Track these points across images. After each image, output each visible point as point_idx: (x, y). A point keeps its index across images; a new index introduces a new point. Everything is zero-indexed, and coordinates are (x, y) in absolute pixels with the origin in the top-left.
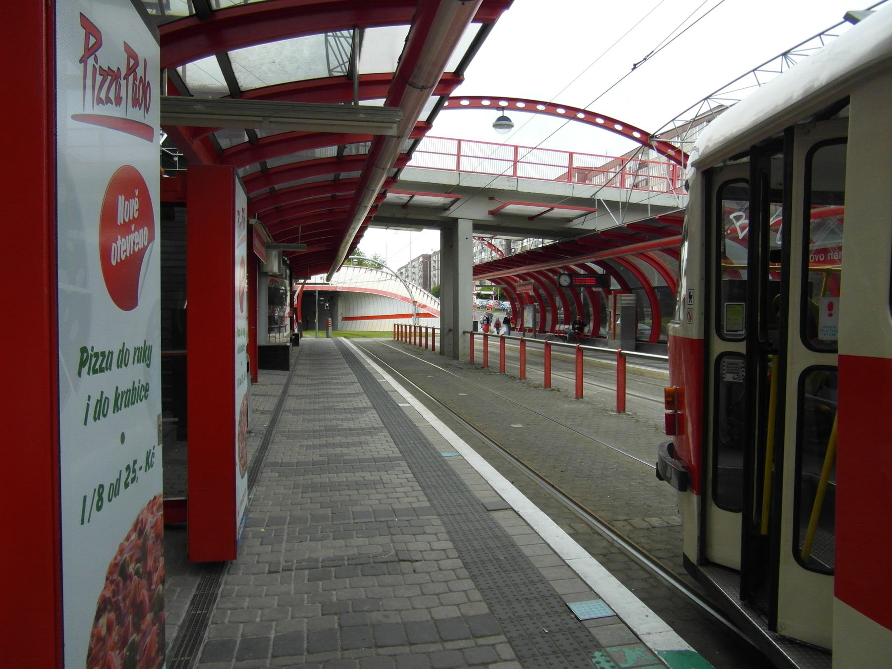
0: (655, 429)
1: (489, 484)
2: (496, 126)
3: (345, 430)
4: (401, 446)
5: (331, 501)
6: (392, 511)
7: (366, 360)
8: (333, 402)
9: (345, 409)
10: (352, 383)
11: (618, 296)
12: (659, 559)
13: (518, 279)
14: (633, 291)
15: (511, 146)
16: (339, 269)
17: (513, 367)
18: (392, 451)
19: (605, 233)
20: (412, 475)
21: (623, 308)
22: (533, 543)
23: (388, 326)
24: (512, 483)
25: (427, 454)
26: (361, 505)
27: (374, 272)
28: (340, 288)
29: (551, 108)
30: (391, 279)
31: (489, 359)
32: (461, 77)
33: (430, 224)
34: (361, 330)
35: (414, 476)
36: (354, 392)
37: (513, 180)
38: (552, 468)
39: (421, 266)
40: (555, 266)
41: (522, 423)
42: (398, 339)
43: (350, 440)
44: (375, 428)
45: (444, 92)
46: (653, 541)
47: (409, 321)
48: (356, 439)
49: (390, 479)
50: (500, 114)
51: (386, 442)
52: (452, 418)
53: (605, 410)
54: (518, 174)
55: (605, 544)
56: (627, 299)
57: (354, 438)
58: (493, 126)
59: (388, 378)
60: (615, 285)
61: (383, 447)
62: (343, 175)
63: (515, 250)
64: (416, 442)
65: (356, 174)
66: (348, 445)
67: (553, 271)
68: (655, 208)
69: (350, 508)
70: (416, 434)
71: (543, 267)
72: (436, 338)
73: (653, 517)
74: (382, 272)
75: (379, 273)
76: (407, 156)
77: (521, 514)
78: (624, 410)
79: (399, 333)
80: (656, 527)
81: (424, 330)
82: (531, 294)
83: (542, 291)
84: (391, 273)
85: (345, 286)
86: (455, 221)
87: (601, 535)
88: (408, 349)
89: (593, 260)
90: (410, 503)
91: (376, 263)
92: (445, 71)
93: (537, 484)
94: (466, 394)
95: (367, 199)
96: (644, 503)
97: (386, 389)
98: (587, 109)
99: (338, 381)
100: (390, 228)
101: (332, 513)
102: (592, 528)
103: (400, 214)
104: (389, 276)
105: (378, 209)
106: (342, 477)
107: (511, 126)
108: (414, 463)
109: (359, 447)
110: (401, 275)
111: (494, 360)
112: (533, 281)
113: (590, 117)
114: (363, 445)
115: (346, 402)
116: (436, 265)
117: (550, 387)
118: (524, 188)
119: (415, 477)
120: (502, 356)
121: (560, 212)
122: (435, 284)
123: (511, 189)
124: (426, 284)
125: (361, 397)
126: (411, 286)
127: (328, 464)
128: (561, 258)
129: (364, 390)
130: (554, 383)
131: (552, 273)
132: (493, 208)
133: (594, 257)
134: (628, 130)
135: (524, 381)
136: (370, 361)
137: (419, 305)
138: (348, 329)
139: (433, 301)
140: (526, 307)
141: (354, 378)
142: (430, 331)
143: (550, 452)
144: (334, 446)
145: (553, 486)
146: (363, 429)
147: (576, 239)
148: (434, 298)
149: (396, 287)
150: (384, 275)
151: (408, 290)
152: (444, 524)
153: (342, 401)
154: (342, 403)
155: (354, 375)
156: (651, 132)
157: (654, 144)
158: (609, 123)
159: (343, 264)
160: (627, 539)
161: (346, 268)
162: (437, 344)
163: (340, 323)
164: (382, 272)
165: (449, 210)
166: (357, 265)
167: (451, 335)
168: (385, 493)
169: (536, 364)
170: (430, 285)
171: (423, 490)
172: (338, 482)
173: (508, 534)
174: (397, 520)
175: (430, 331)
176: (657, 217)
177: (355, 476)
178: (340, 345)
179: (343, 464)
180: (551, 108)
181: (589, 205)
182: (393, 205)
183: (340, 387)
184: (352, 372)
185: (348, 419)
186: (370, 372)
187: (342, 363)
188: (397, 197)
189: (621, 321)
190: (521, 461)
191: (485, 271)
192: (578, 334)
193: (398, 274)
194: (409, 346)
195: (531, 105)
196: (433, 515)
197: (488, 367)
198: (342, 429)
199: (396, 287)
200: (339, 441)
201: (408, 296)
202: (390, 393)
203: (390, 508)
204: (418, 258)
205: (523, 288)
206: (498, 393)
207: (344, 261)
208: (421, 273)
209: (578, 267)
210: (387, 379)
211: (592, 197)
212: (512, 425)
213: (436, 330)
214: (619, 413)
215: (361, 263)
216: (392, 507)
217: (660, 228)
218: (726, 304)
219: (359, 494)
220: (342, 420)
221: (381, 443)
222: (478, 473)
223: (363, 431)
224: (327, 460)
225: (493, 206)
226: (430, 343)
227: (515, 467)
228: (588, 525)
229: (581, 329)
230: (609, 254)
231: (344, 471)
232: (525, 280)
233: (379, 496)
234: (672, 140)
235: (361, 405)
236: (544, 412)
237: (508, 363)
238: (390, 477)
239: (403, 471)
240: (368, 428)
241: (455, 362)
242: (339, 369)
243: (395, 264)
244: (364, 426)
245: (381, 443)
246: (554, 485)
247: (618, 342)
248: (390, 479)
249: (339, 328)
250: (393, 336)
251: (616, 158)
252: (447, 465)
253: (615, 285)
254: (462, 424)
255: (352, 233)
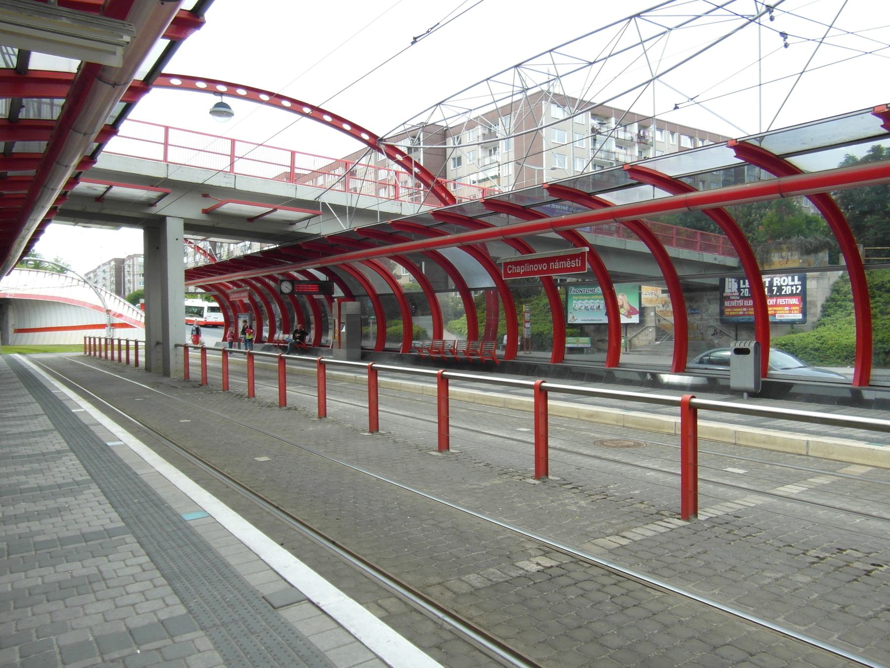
0: (417, 450)
1: (262, 560)
2: (213, 112)
3: (32, 490)
4: (121, 510)
5: (17, 631)
6: (128, 632)
7: (52, 382)
8: (9, 446)
9: (29, 456)
10: (36, 415)
11: (343, 303)
12: (505, 639)
13: (231, 286)
14: (356, 298)
15: (227, 138)
16: (9, 273)
17: (239, 383)
18: (98, 501)
19: (332, 238)
20: (147, 558)
21: (348, 316)
22: (360, 661)
23: (77, 338)
24: (282, 545)
25: (162, 518)
26: (73, 629)
27: (56, 276)
28: (11, 295)
29: (276, 99)
30: (78, 284)
31: (208, 375)
32: (201, 18)
33: (132, 222)
34: (40, 343)
35: (150, 558)
36: (40, 429)
37: (230, 176)
38: (324, 516)
39: (113, 272)
40: (275, 272)
41: (267, 454)
42: (90, 354)
43: (40, 506)
44: (78, 483)
45: (176, 35)
46: (485, 612)
47: (103, 333)
48: (51, 504)
49: (115, 570)
50: (218, 99)
51: (97, 503)
52: (179, 454)
53: (355, 430)
54: (236, 171)
55: (431, 627)
56: (351, 307)
57: (47, 502)
58: (210, 113)
59: (85, 406)
60: (338, 292)
61: (95, 513)
62: (19, 147)
63: (221, 255)
64: (142, 500)
65: (38, 147)
66: (40, 516)
67: (271, 277)
68: (384, 215)
69: (53, 638)
70: (139, 487)
71: (260, 273)
72: (139, 350)
73: (469, 573)
74: (66, 277)
75: (62, 278)
76: (111, 130)
77: (323, 608)
78: (377, 430)
79: (90, 347)
80: (479, 589)
81: (116, 342)
82: (245, 302)
83: (258, 298)
84: (78, 278)
85: (18, 292)
86: (162, 219)
87: (421, 613)
88: (105, 366)
89: (319, 266)
90: (154, 612)
91: (58, 266)
92: (182, 8)
93: (314, 543)
94: (188, 421)
95: (48, 195)
96: (451, 553)
97: (86, 422)
98: (299, 116)
99: (15, 414)
100: (79, 224)
101: (21, 657)
102: (406, 604)
103: (94, 208)
104: (75, 282)
105: (67, 198)
106: (35, 578)
107: (230, 114)
108: (146, 536)
109: (57, 517)
110: (89, 279)
111: (215, 377)
112: (248, 288)
113: (317, 113)
114: (62, 513)
115: (30, 444)
116: (131, 270)
117: (285, 406)
118: (242, 186)
119: (152, 561)
120: (225, 372)
121: (283, 214)
122: (130, 291)
123: (228, 186)
124: (119, 289)
125: (50, 436)
126: (103, 293)
127: (9, 555)
128: (281, 264)
129: (54, 424)
130: (289, 401)
131: (255, 281)
132: (206, 207)
133: (320, 263)
134: (356, 131)
135: (253, 399)
136: (57, 384)
137: (114, 315)
138: (23, 342)
139: (131, 310)
140: (240, 316)
141: (37, 408)
142: (132, 344)
143: (314, 492)
144: (16, 519)
145: (334, 543)
146: (60, 486)
147: (300, 243)
148: (131, 306)
149: (86, 294)
150: (69, 280)
151: (100, 298)
152: (217, 646)
153: (23, 444)
154: (23, 447)
155: (37, 404)
156: (380, 135)
157: (382, 147)
158: (337, 122)
159: (15, 266)
160: (454, 613)
162: (142, 359)
163: (12, 336)
164: (66, 277)
165: (156, 206)
166: (33, 268)
167: (159, 348)
168: (110, 598)
169: (268, 378)
170: (124, 292)
171: (170, 585)
172: (29, 589)
173: (319, 650)
174: (139, 652)
175: (132, 344)
176: (390, 222)
177: (56, 572)
178: (14, 364)
179: (33, 553)
180: (276, 99)
181: (314, 207)
182: (83, 197)
183: (19, 422)
184: (34, 400)
185: (34, 471)
186: (61, 398)
187: (18, 389)
188: (89, 187)
189: (347, 329)
190: (282, 509)
191: (195, 277)
192: (299, 343)
193: (85, 278)
194: (105, 362)
195: (253, 93)
196: (195, 630)
197: (207, 384)
198: (26, 489)
199: (86, 294)
200: (23, 510)
201: (100, 304)
202: (92, 428)
203: (124, 629)
204: (109, 262)
205: (237, 295)
206: (227, 416)
207: (17, 263)
208: (113, 279)
209: (302, 274)
210: (84, 408)
211: (315, 199)
212: (256, 459)
213: (130, 342)
214: (372, 433)
215: (38, 266)
216: (125, 624)
217: (390, 234)
219: (66, 607)
220: (26, 474)
221: (91, 508)
222: (242, 543)
223: (60, 489)
224: (5, 547)
225: (208, 204)
226: (132, 357)
227: (277, 519)
228: (400, 599)
229: (302, 338)
230: (334, 261)
231: (37, 564)
232: (239, 286)
233: (102, 607)
234: (399, 143)
235: (52, 449)
236: (289, 438)
237: (232, 379)
238: (116, 565)
239: (132, 552)
240: (68, 484)
241: (165, 380)
242: (15, 396)
243: (81, 265)
244: (60, 481)
245: (91, 508)
246: (334, 540)
247: (343, 352)
248: (115, 570)
249: (10, 342)
250: (83, 350)
251: (337, 160)
252: (194, 533)
253: (338, 292)
254: (194, 462)
255: (27, 235)
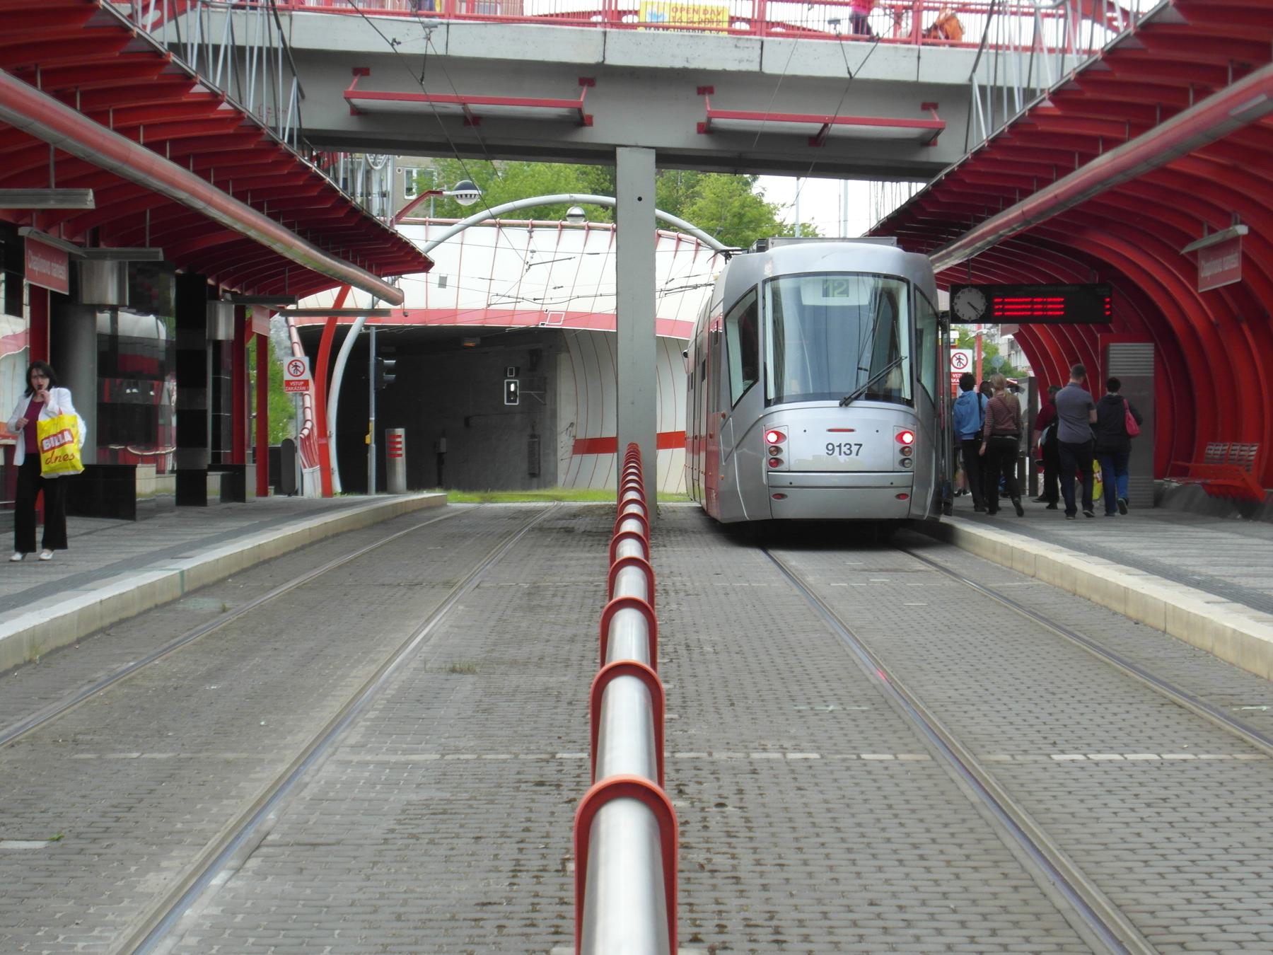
37: (748, 44)
123: (744, 67)
161: (555, 232)
218: (517, 404)
